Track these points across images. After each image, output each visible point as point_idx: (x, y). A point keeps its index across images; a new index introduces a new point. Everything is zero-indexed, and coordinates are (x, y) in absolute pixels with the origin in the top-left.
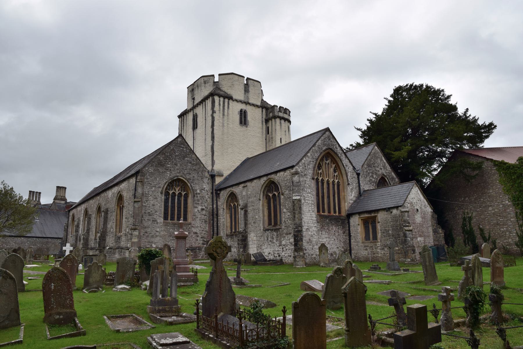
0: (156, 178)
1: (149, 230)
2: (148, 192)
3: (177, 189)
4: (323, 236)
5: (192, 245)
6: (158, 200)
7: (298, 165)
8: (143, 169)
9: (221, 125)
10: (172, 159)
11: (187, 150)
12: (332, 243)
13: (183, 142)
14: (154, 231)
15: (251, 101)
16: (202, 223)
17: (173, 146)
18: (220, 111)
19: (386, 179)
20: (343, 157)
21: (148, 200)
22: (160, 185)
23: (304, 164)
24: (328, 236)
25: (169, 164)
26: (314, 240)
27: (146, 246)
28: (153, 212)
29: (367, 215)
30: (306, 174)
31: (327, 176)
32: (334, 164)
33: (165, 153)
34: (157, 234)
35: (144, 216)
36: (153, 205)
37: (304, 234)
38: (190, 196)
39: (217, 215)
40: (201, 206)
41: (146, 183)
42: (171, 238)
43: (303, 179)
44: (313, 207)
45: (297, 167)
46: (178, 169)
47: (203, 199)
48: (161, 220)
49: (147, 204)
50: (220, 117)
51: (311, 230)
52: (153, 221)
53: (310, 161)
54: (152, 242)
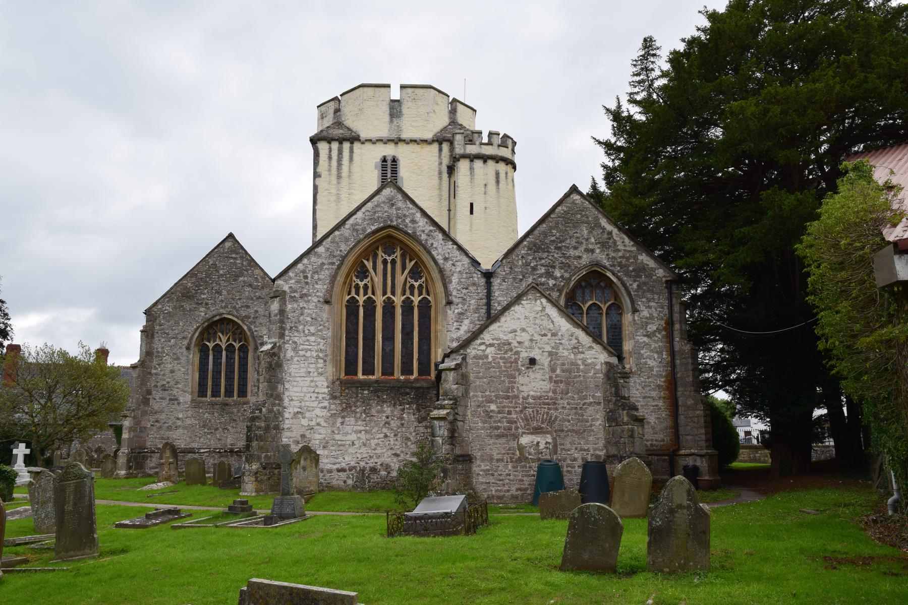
0: (177, 323)
1: (162, 417)
2: (163, 348)
4: (348, 429)
6: (182, 361)
8: (153, 309)
9: (333, 198)
10: (211, 283)
12: (377, 445)
13: (235, 247)
14: (172, 418)
15: (405, 136)
17: (215, 259)
18: (330, 170)
19: (609, 274)
20: (437, 241)
21: (163, 363)
22: (185, 333)
23: (304, 272)
24: (363, 428)
25: (204, 294)
26: (317, 436)
27: (156, 445)
28: (172, 383)
30: (306, 295)
33: (196, 274)
34: (179, 423)
35: (154, 392)
36: (172, 372)
37: (287, 424)
41: (157, 333)
42: (206, 430)
43: (295, 305)
44: (320, 365)
46: (222, 301)
48: (186, 398)
49: (159, 369)
50: (330, 182)
51: (308, 415)
52: (170, 400)
53: (323, 264)
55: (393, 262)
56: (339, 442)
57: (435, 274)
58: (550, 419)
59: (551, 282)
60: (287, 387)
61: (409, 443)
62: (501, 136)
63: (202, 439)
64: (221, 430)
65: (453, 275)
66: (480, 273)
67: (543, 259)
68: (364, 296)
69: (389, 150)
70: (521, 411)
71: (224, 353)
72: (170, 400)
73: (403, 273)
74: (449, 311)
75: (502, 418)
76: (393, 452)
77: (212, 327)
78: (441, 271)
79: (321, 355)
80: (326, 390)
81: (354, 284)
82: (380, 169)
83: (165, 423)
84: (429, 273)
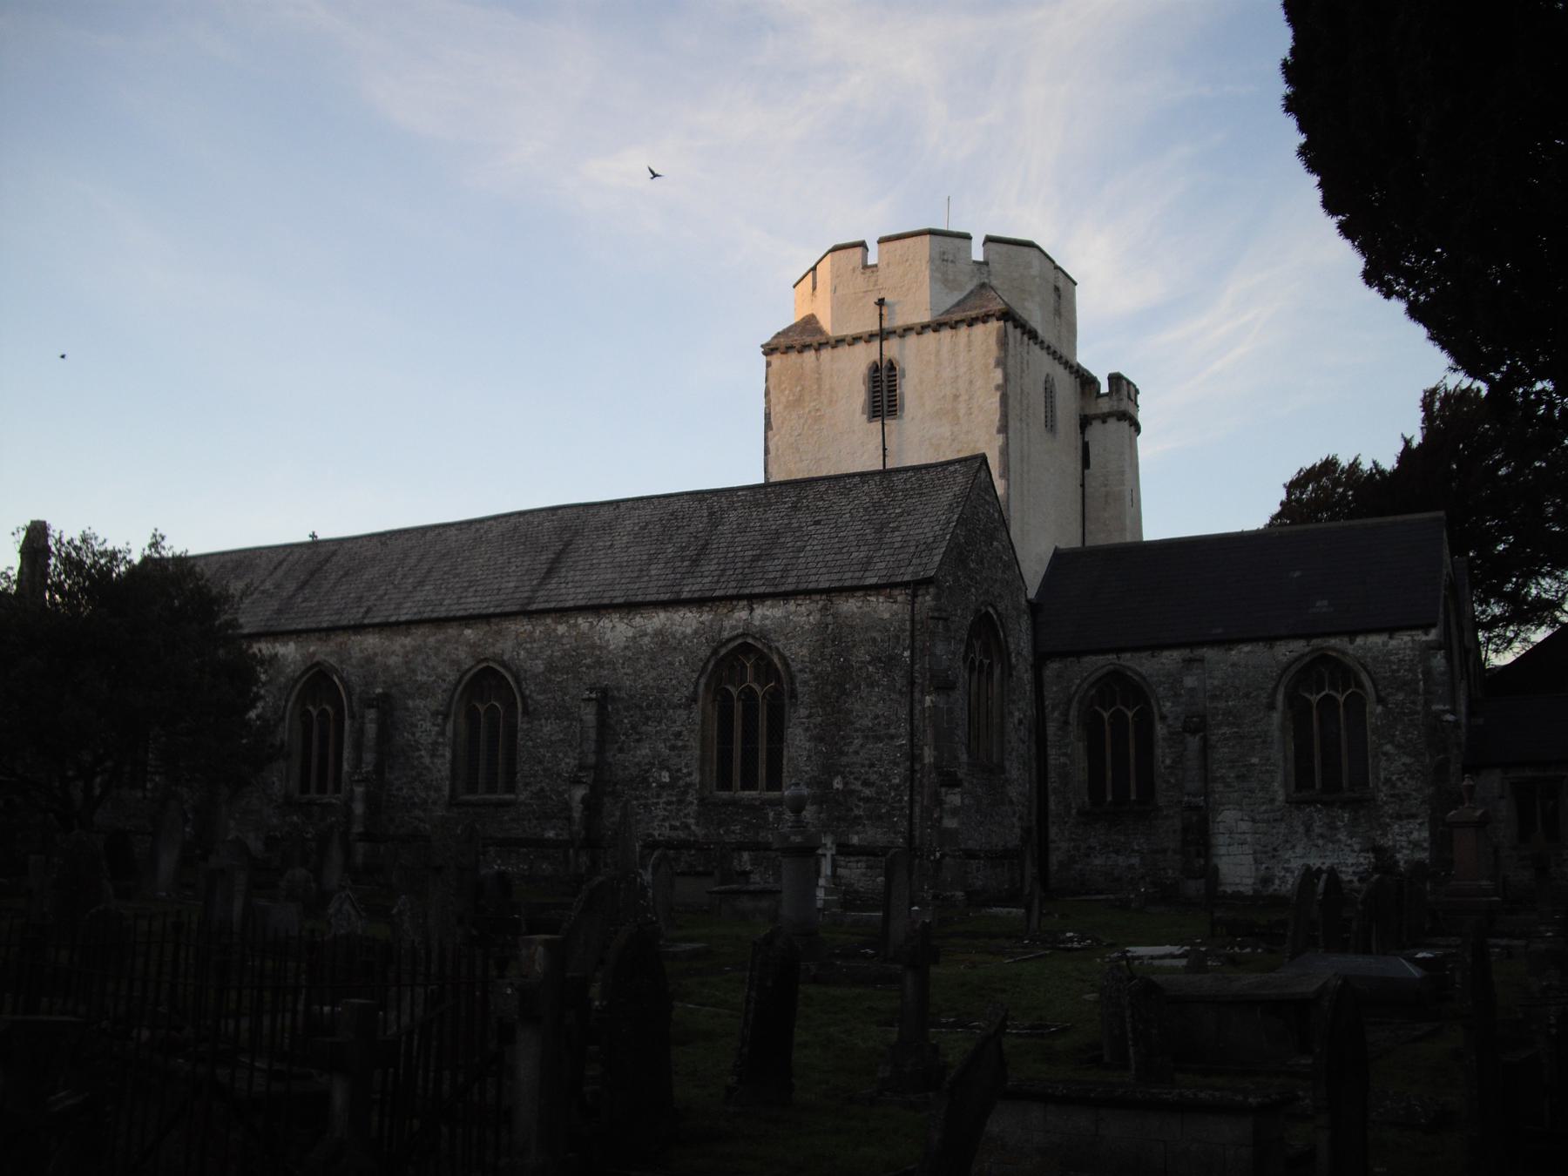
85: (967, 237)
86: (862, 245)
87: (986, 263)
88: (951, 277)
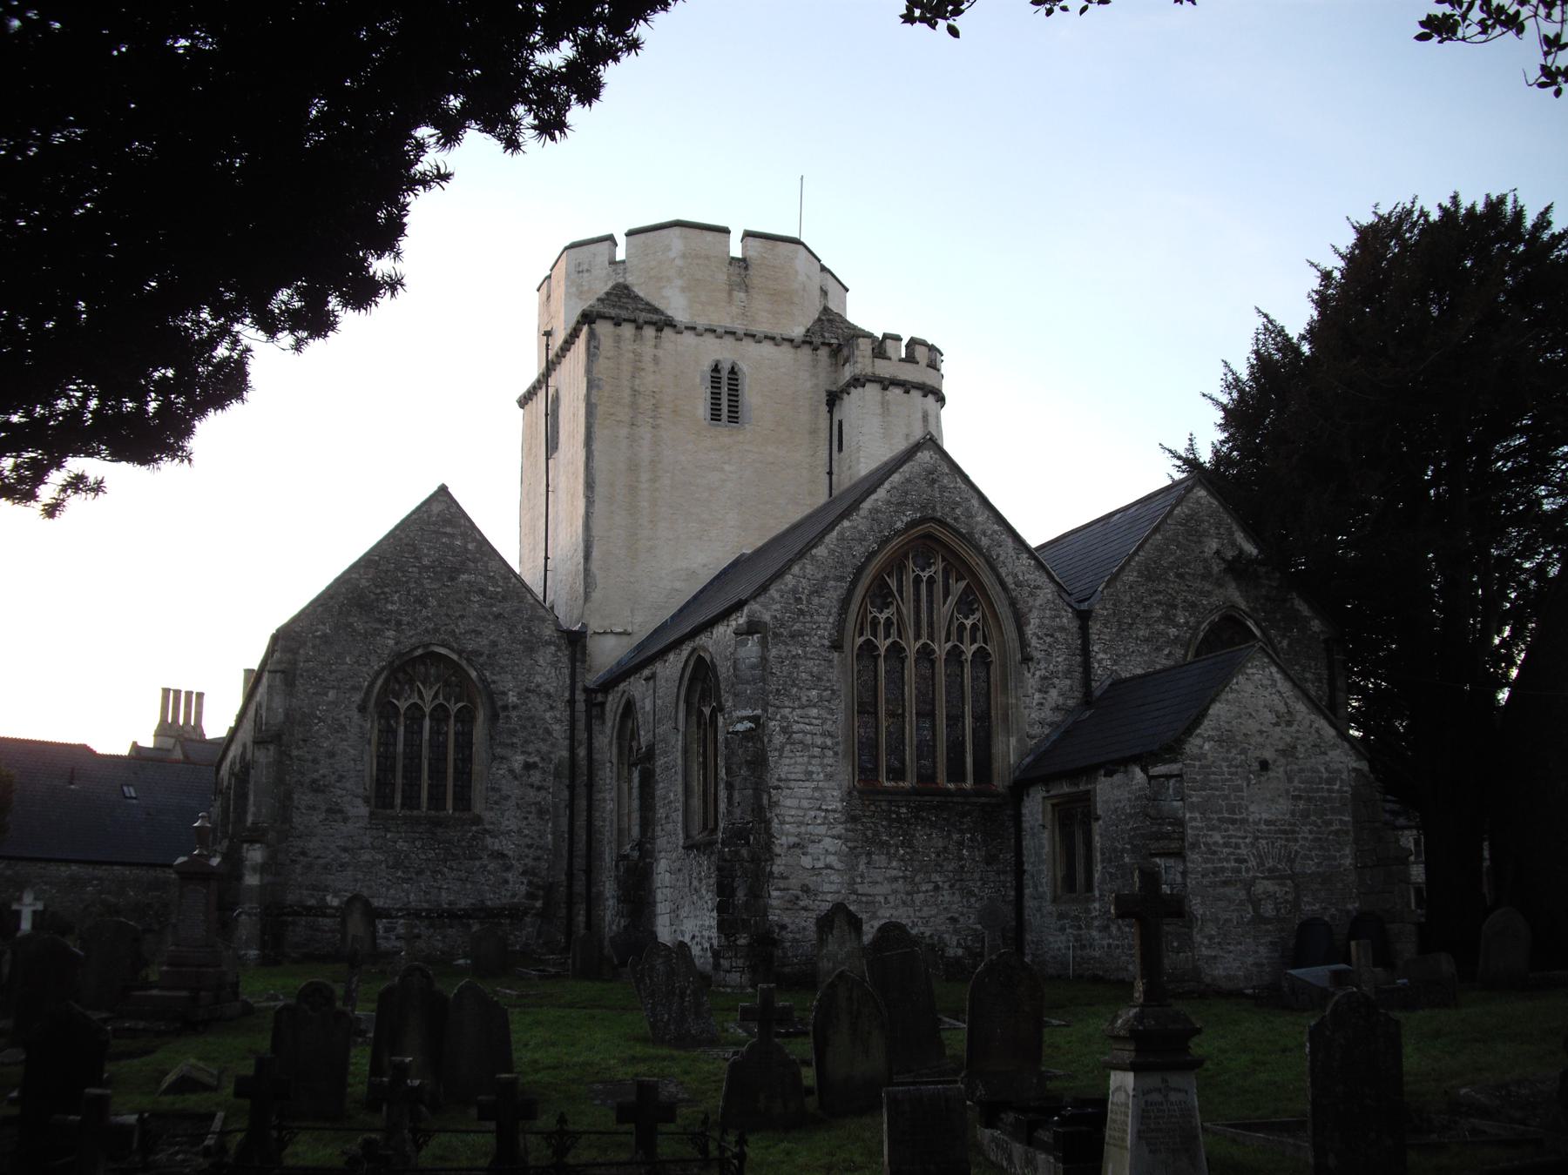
3: (428, 695)
5: (482, 901)
7: (761, 599)
11: (467, 543)
16: (526, 818)
23: (794, 591)
25: (393, 603)
29: (1066, 789)
30: (800, 634)
31: (924, 631)
32: (963, 578)
34: (346, 857)
36: (332, 755)
38: (481, 716)
39: (590, 786)
40: (523, 753)
41: (302, 676)
45: (754, 606)
47: (534, 726)
51: (811, 849)
54: (326, 889)
55: (931, 581)
56: (864, 899)
57: (1004, 610)
58: (1289, 856)
59: (1173, 631)
60: (775, 799)
61: (973, 900)
62: (904, 343)
63: (392, 891)
64: (429, 873)
65: (1030, 611)
66: (1070, 610)
67: (1160, 592)
68: (885, 639)
69: (724, 351)
70: (1253, 844)
71: (427, 723)
72: (329, 811)
73: (944, 603)
74: (1026, 673)
75: (1228, 854)
76: (949, 915)
77: (404, 669)
78: (1013, 603)
79: (829, 742)
80: (839, 806)
81: (870, 617)
82: (709, 384)
83: (319, 857)
84: (991, 605)
85: (725, 231)
86: (610, 239)
87: (744, 260)
88: (586, 288)
